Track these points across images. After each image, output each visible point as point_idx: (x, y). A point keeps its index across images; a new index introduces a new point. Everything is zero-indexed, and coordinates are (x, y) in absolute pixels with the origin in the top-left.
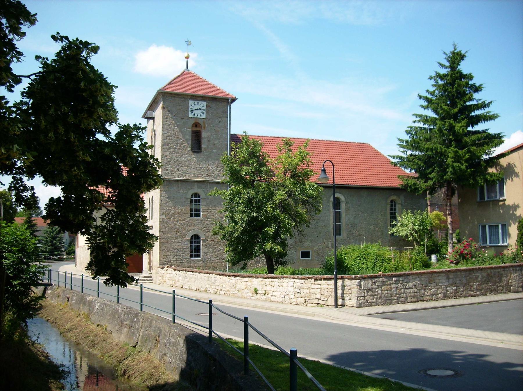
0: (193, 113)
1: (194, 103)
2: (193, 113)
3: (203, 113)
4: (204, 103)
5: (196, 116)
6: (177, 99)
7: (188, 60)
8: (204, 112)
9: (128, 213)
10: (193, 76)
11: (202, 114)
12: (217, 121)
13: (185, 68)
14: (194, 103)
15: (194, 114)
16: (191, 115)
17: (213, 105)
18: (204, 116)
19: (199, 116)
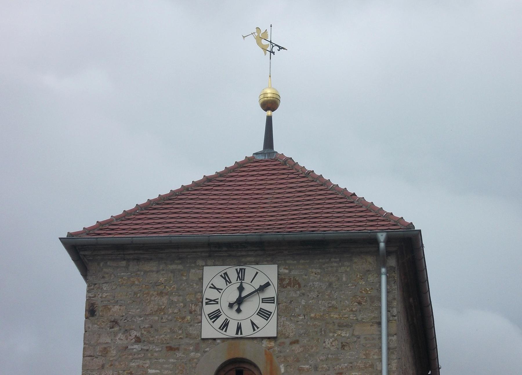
0: (220, 321)
1: (225, 277)
2: (220, 321)
3: (264, 314)
4: (269, 273)
5: (231, 332)
6: (152, 266)
7: (275, 115)
8: (271, 307)
9: (387, 268)
10: (287, 166)
11: (259, 321)
12: (330, 343)
13: (260, 147)
14: (225, 277)
15: (225, 325)
16: (209, 330)
17: (313, 274)
18: (269, 328)
19: (247, 331)
